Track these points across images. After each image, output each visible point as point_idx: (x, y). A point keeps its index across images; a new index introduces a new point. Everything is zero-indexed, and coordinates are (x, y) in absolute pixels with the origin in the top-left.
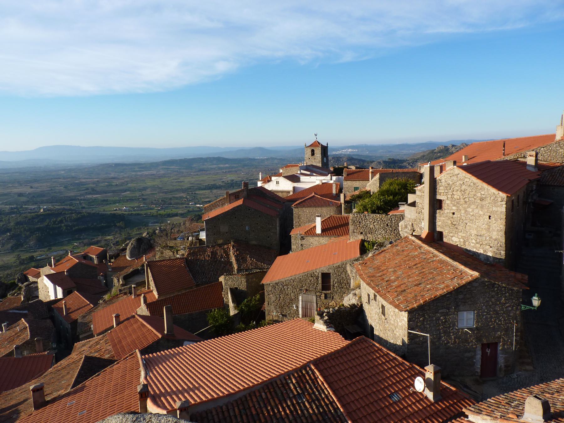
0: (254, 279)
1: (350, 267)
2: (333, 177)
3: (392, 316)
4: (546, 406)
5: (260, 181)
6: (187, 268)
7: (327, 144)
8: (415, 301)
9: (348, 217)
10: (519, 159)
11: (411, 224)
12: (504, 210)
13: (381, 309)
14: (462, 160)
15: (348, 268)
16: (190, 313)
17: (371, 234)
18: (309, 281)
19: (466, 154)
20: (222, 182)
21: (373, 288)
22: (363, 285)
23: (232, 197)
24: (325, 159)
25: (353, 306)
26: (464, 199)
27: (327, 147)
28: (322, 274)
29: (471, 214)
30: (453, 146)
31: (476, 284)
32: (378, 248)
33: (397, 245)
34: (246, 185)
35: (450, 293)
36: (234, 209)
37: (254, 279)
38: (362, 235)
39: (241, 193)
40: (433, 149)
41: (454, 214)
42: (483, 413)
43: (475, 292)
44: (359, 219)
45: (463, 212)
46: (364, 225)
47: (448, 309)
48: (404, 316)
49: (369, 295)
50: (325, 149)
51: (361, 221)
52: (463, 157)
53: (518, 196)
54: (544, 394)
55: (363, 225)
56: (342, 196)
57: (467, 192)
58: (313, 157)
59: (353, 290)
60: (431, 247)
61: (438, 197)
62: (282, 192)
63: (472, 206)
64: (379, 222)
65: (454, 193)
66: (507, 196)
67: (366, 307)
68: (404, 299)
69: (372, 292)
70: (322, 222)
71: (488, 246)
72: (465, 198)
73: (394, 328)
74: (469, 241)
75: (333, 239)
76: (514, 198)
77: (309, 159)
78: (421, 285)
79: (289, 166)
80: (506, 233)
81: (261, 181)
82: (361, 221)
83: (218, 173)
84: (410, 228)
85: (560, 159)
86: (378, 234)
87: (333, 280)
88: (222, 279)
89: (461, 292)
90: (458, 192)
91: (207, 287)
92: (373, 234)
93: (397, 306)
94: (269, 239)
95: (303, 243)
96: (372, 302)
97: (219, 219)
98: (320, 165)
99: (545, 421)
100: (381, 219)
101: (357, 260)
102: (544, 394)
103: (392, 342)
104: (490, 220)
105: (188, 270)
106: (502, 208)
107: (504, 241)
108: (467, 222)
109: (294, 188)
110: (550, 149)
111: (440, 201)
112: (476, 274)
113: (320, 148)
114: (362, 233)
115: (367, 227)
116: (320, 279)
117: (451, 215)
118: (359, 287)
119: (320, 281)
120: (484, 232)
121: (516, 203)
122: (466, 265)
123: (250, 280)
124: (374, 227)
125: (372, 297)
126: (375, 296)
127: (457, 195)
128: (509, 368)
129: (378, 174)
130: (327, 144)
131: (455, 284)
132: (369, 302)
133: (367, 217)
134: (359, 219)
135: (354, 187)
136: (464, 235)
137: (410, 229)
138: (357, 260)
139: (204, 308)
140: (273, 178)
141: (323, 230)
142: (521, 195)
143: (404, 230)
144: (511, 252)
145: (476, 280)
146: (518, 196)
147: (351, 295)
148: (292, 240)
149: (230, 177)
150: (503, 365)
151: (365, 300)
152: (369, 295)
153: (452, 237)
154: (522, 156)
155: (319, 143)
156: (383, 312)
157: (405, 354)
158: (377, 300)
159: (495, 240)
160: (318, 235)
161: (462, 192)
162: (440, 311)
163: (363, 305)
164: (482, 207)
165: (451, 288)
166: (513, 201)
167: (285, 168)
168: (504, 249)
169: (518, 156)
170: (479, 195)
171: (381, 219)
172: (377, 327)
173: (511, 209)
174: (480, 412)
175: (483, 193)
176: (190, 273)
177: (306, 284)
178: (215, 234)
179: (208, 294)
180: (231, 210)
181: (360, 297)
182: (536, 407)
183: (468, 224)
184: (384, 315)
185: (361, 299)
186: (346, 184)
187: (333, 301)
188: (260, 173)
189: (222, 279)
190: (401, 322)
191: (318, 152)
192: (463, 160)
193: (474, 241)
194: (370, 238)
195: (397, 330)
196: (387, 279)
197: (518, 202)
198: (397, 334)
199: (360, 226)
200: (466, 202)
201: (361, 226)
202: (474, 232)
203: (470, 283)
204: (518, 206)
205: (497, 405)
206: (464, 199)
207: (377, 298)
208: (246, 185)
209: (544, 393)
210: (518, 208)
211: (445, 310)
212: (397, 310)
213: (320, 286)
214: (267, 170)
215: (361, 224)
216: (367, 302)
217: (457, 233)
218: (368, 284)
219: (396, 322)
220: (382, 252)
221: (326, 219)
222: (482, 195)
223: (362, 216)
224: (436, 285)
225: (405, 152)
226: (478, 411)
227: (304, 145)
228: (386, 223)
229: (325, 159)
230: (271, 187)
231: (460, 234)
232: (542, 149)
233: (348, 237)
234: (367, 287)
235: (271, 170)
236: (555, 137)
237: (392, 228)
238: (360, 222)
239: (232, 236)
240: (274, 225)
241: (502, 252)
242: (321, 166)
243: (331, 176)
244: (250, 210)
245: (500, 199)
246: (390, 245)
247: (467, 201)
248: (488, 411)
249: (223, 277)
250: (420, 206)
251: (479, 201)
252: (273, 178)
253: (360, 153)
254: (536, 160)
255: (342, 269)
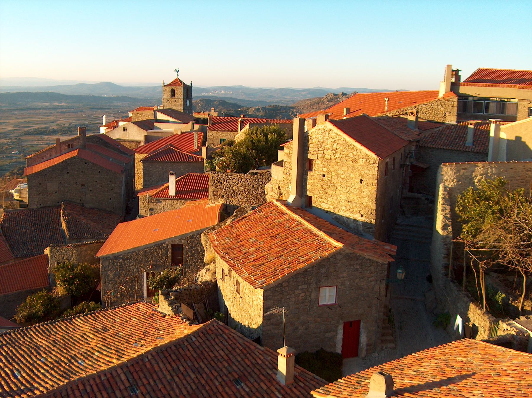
0: (89, 252)
1: (205, 237)
2: (195, 125)
3: (247, 294)
4: (389, 382)
5: (103, 126)
6: (3, 237)
7: (191, 84)
8: (273, 276)
9: (207, 176)
10: (401, 116)
11: (277, 187)
12: (376, 173)
13: (236, 287)
14: (343, 113)
15: (203, 239)
16: (4, 294)
17: (234, 197)
18: (156, 254)
19: (348, 107)
20: (57, 125)
21: (227, 262)
22: (218, 259)
23: (65, 147)
24: (188, 101)
25: (206, 283)
26: (335, 159)
27: (191, 87)
28: (172, 245)
29: (343, 176)
30: (344, 94)
31: (340, 257)
32: (238, 215)
33: (260, 211)
34: (83, 131)
35: (312, 266)
36: (65, 161)
37: (89, 252)
38: (224, 198)
39: (75, 141)
40: (321, 97)
41: (324, 176)
42: (330, 394)
43: (338, 265)
44: (220, 179)
45: (334, 174)
46: (227, 186)
47: (309, 284)
48: (260, 292)
49: (223, 270)
50: (188, 90)
51: (223, 181)
52: (345, 109)
53: (394, 158)
54: (395, 371)
55: (225, 186)
56: (204, 149)
57: (339, 151)
58: (173, 99)
59: (208, 264)
60: (297, 214)
61: (310, 157)
62: (130, 142)
63: (344, 169)
64: (244, 183)
65: (325, 152)
66: (379, 159)
67: (220, 283)
68: (262, 273)
69: (226, 267)
70: (176, 182)
71: (358, 214)
72: (336, 158)
73: (248, 308)
74: (339, 208)
75: (189, 204)
76: (388, 160)
77: (168, 101)
78: (282, 257)
79: (141, 109)
80: (377, 200)
81: (105, 126)
82: (223, 181)
83: (51, 113)
84: (276, 190)
85: (441, 119)
86: (242, 198)
87: (186, 253)
88: (47, 251)
89: (324, 265)
90: (330, 151)
91: (29, 261)
92: (236, 197)
93: (252, 283)
94: (111, 201)
95: (152, 207)
96: (227, 278)
97: (46, 174)
98: (181, 109)
99: (387, 397)
100: (246, 180)
101: (213, 228)
102: (395, 371)
103: (246, 324)
104: (361, 184)
105: (4, 239)
106: (374, 171)
107: (375, 208)
108: (337, 185)
109: (146, 137)
110: (432, 107)
111: (311, 161)
112: (340, 245)
113: (182, 88)
114: (223, 196)
115: (229, 188)
116: (170, 250)
117: (321, 176)
118: (214, 261)
119: (170, 255)
120: (355, 197)
121: (390, 166)
122: (330, 235)
123: (83, 253)
124: (238, 189)
125: (226, 272)
126: (230, 271)
127: (328, 154)
128: (372, 347)
129: (248, 124)
130: (191, 84)
131: (316, 256)
132: (223, 279)
133: (230, 177)
134: (220, 179)
135: (221, 139)
136: (334, 200)
137: (276, 193)
138: (213, 228)
139: (24, 287)
140: (121, 124)
141: (177, 192)
142: (398, 157)
143: (271, 195)
144: (383, 221)
145: (339, 252)
146: (394, 158)
147: (203, 271)
148: (140, 203)
149: (64, 121)
150: (365, 344)
151: (219, 276)
152: (223, 270)
153: (322, 202)
154: (404, 113)
155: (181, 81)
156: (238, 290)
157: (259, 337)
158: (232, 276)
159: (366, 207)
160: (171, 198)
161: (334, 151)
162: (300, 287)
163: (218, 283)
164: (354, 168)
165: (312, 262)
166: (387, 164)
167: (135, 111)
168: (374, 217)
169: (400, 112)
170: (351, 155)
171: (246, 180)
172: (232, 308)
173: (384, 173)
174: (328, 393)
175: (355, 153)
176: (6, 243)
177: (152, 258)
178: (40, 194)
179: (29, 270)
180: (62, 163)
181: (215, 273)
182: (379, 384)
183: (338, 188)
184: (239, 293)
185: (215, 276)
186: (210, 134)
187: (185, 278)
188: (104, 117)
189: (47, 251)
190: (257, 300)
191: (179, 92)
192: (345, 114)
193: (344, 208)
194: (234, 202)
195: (252, 309)
196: (244, 251)
197: (394, 165)
198: (253, 314)
199: (221, 188)
200: (337, 163)
201: (222, 187)
202: (344, 198)
203: (334, 256)
204: (394, 169)
205: (346, 385)
206: (335, 159)
207: (232, 273)
208: (83, 131)
209: (394, 369)
210: (393, 171)
211: (305, 286)
212: (252, 287)
213: (169, 260)
214: (117, 112)
215: (223, 185)
216: (222, 278)
217: (326, 198)
218: (222, 257)
219: (251, 301)
220: (243, 218)
221: (182, 178)
222: (354, 156)
223: (224, 175)
224: (299, 257)
225: (288, 98)
226: (326, 392)
227: (162, 82)
228: (252, 184)
229: (188, 101)
230: (116, 135)
231: (329, 199)
232: (424, 106)
233: (206, 201)
234: (222, 261)
235: (121, 112)
236: (438, 94)
237: (258, 191)
238: (221, 183)
239: (63, 197)
240: (118, 183)
241: (372, 220)
242: (182, 111)
243: (193, 124)
244: (87, 164)
245: (372, 162)
246: (252, 211)
247: (339, 161)
248: (336, 392)
249: (48, 248)
250: (288, 166)
251: (351, 162)
252: (121, 124)
253: (234, 96)
254: (417, 118)
255: (195, 237)
